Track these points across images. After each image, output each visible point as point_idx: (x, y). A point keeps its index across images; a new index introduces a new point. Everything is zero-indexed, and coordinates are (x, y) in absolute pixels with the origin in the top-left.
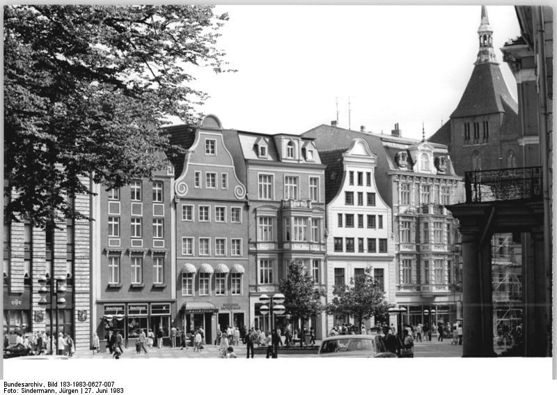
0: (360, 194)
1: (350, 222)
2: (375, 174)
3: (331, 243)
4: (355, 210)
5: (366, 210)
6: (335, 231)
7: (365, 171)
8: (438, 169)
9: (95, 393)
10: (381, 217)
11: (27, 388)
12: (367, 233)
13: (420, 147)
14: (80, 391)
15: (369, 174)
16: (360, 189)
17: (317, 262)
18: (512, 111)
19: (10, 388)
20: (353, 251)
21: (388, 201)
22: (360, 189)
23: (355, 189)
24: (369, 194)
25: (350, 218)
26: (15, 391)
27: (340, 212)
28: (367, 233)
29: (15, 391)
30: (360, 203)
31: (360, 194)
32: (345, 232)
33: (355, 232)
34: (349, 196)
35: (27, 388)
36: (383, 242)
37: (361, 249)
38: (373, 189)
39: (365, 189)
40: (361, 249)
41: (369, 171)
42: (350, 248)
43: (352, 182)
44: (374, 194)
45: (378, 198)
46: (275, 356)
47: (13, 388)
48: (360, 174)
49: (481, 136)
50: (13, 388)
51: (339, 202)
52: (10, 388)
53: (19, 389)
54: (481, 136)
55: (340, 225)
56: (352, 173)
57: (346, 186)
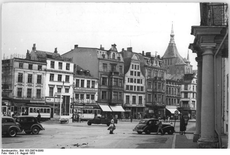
0: (135, 72)
1: (132, 81)
2: (140, 66)
3: (125, 87)
4: (134, 77)
5: (137, 78)
6: (127, 83)
7: (137, 64)
8: (160, 66)
9: (20, 154)
10: (142, 80)
11: (11, 152)
12: (137, 85)
13: (155, 59)
14: (15, 153)
15: (138, 66)
16: (135, 70)
17: (120, 93)
18: (138, 146)
19: (4, 152)
20: (132, 90)
21: (144, 75)
22: (135, 70)
23: (134, 70)
24: (138, 72)
25: (132, 80)
26: (6, 153)
27: (129, 77)
28: (137, 85)
29: (6, 153)
30: (135, 75)
31: (135, 72)
32: (130, 84)
33: (133, 84)
34: (132, 72)
35: (11, 152)
36: (142, 87)
37: (135, 90)
38: (139, 71)
39: (137, 71)
40: (135, 90)
41: (138, 65)
42: (131, 89)
43: (133, 68)
44: (140, 72)
45: (141, 74)
46: (3, 88)
47: (6, 152)
48: (135, 66)
49: (170, 64)
50: (6, 152)
51: (128, 74)
52: (4, 152)
53: (8, 152)
54: (170, 64)
55: (128, 82)
56: (133, 65)
57: (131, 69)
